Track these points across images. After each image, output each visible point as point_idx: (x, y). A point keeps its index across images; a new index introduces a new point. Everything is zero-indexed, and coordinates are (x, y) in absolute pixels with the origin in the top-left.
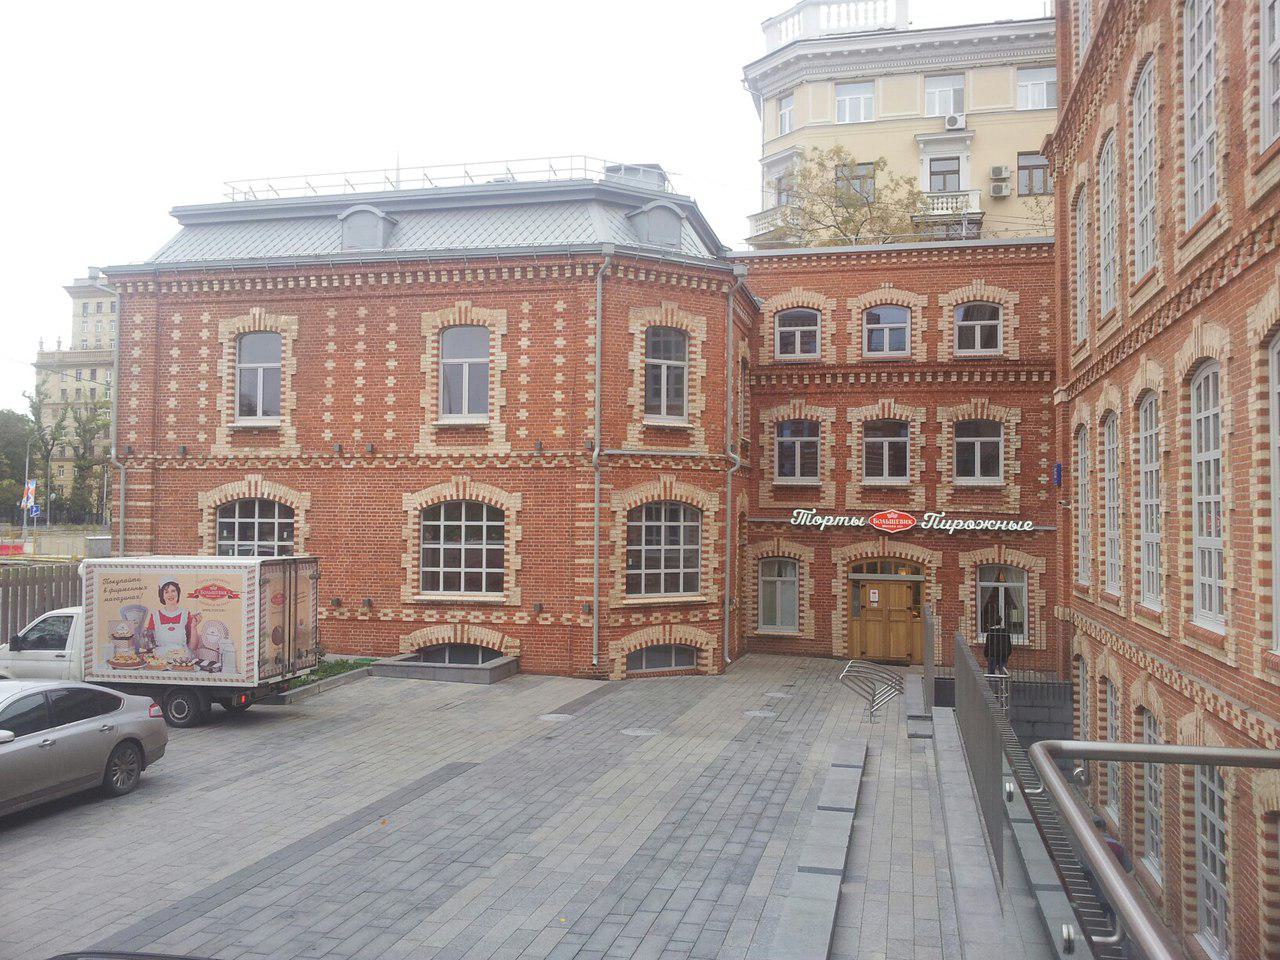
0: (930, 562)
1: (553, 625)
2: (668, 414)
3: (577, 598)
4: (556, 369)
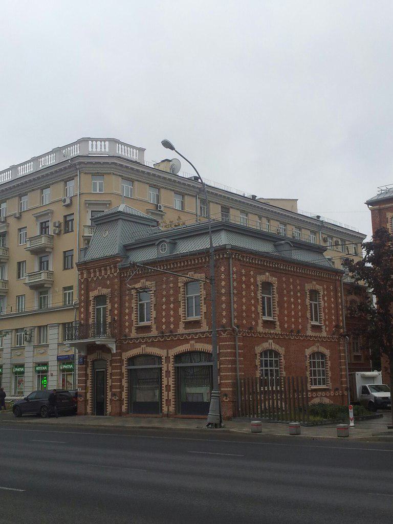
2: (315, 321)
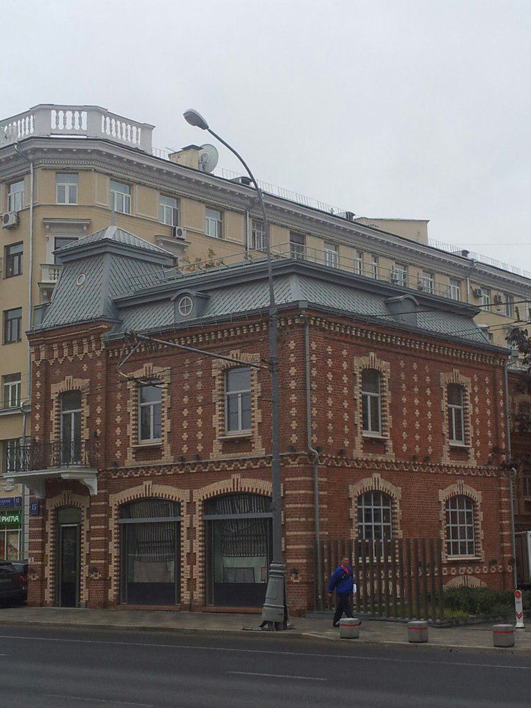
2: (372, 430)
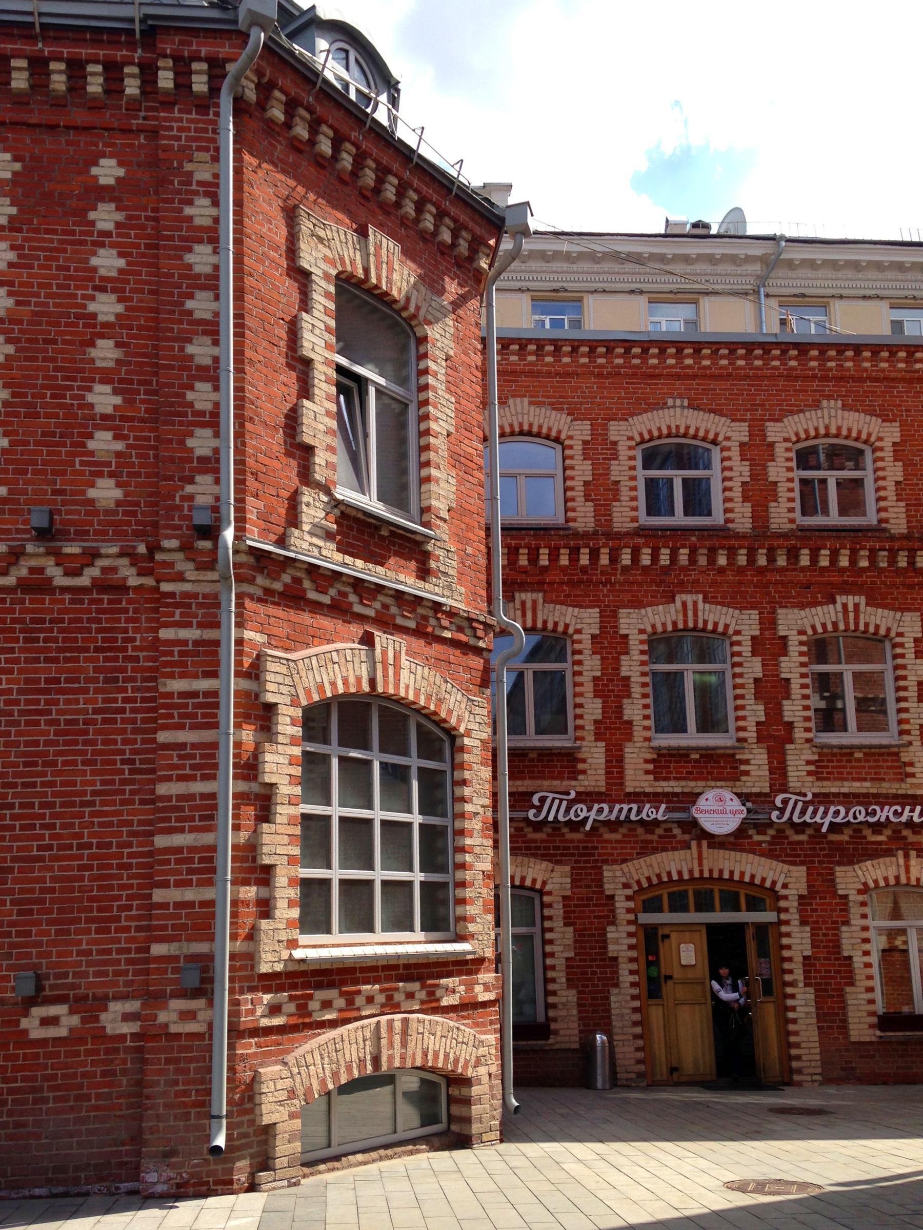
0: (785, 886)
1: (75, 1038)
3: (157, 949)
4: (96, 330)
